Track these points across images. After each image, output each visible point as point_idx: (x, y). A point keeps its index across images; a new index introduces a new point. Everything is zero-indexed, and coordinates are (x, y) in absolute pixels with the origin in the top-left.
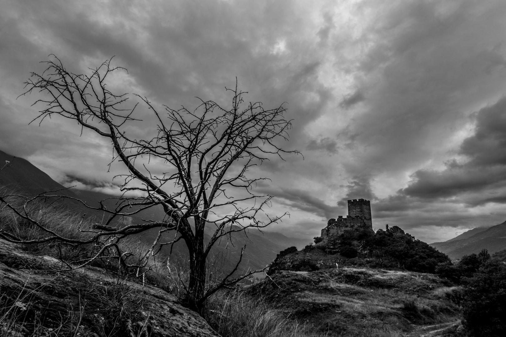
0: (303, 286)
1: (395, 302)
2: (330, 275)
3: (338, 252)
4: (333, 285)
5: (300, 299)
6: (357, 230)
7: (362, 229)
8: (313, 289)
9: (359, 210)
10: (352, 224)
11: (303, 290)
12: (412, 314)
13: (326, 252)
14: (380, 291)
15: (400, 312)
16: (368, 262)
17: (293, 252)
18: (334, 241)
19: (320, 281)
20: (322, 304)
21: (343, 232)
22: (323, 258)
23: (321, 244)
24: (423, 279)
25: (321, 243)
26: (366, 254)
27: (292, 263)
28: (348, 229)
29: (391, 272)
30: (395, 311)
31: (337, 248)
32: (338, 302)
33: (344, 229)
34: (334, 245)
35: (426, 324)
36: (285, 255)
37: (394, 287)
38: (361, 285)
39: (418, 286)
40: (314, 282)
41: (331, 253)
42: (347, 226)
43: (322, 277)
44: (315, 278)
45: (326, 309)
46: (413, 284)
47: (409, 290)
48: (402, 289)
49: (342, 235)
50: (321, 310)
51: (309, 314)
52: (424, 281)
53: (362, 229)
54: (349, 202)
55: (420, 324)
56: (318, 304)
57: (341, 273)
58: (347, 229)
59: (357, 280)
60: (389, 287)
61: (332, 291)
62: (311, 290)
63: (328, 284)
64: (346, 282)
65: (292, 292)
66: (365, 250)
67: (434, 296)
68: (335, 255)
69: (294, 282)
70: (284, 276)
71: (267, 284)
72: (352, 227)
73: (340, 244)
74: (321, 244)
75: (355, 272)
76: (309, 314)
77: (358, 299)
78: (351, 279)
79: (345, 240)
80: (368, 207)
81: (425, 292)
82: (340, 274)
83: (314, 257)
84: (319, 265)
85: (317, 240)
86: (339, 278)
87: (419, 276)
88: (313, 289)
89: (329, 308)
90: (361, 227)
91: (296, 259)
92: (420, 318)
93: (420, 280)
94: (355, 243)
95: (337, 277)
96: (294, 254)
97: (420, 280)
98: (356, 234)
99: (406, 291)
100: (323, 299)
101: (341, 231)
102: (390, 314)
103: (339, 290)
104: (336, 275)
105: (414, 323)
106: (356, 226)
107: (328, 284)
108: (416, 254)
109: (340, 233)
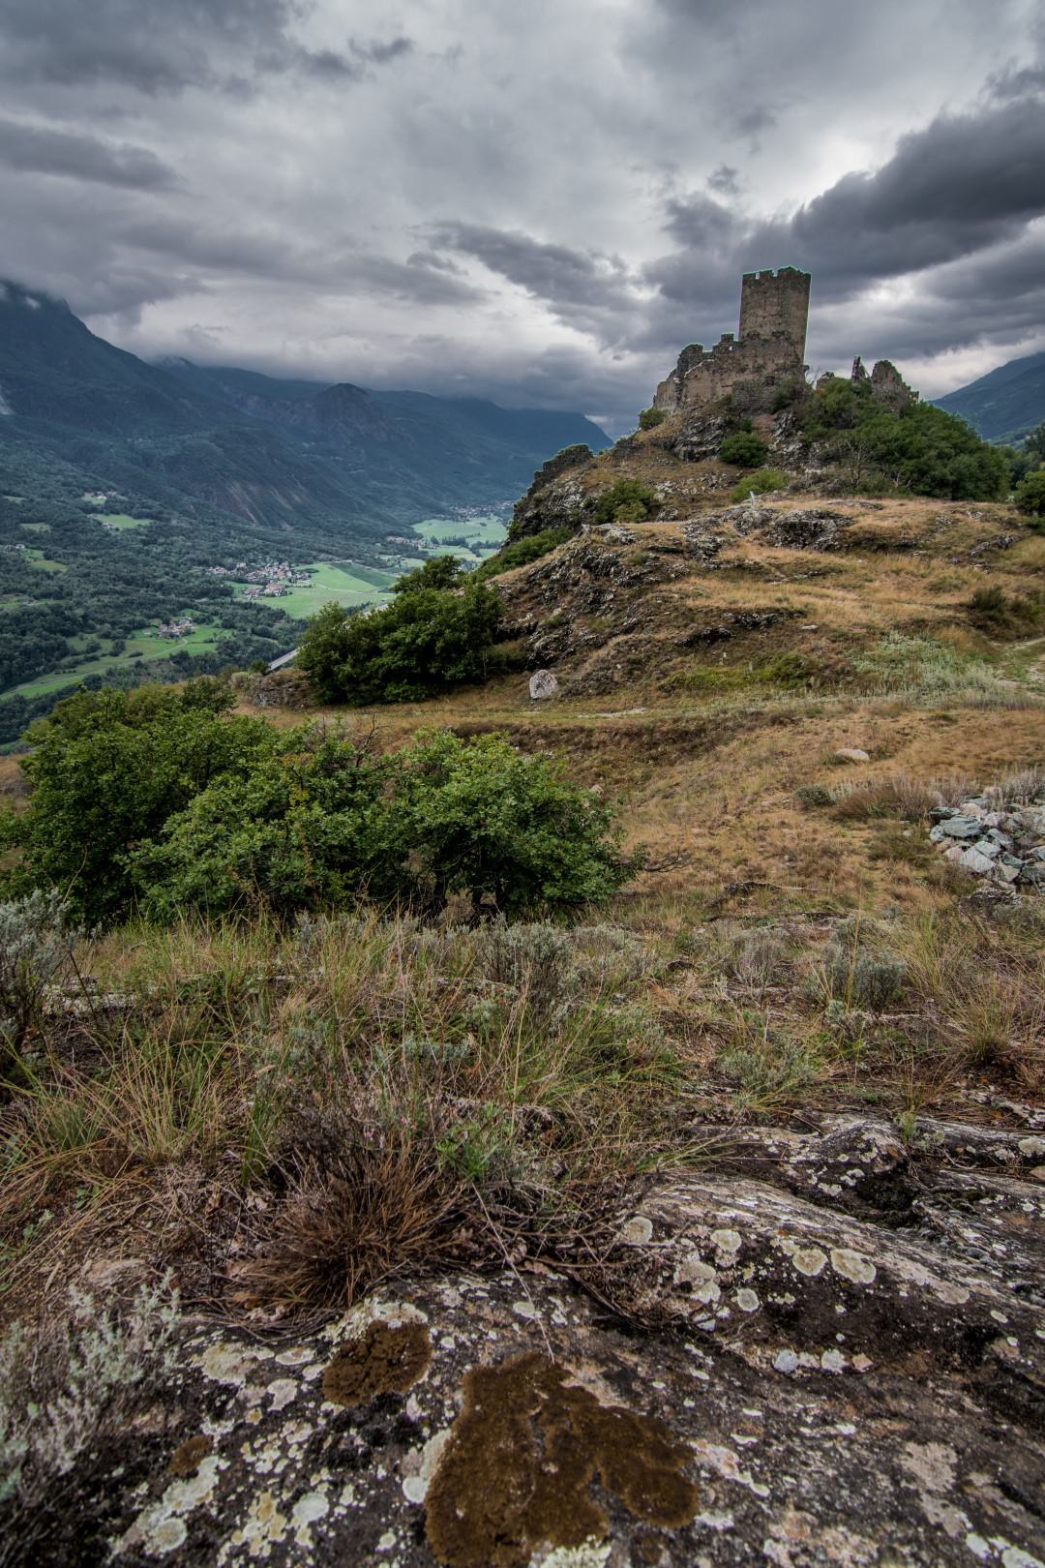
0: (678, 563)
1: (937, 588)
2: (739, 526)
3: (713, 452)
4: (755, 554)
5: (690, 603)
6: (771, 381)
7: (787, 377)
8: (708, 570)
9: (775, 310)
10: (760, 361)
11: (681, 576)
12: (991, 618)
13: (676, 455)
14: (889, 561)
15: (962, 615)
16: (818, 480)
17: (581, 462)
18: (703, 420)
19: (718, 546)
20: (759, 611)
21: (729, 390)
22: (666, 473)
23: (658, 431)
24: (984, 519)
25: (662, 427)
26: (792, 454)
27: (583, 495)
28: (747, 377)
29: (892, 505)
30: (951, 613)
31: (710, 443)
32: (797, 602)
33: (735, 377)
34: (701, 432)
35: (1019, 638)
36: (559, 472)
37: (916, 547)
38: (829, 549)
39: (980, 541)
40: (706, 551)
41: (691, 457)
42: (743, 370)
43: (720, 534)
44: (704, 539)
45: (769, 623)
46: (963, 537)
47: (957, 554)
48: (935, 551)
49: (728, 399)
50: (756, 625)
51: (726, 637)
52: (987, 525)
53: (787, 377)
54: (748, 280)
55: (1009, 640)
56: (749, 613)
57: (769, 520)
58: (742, 378)
59: (815, 535)
60: (904, 548)
61: (757, 572)
62: (704, 573)
63: (740, 552)
64: (787, 544)
65: (651, 583)
66: (788, 444)
67: (1023, 565)
68: (704, 464)
69: (652, 555)
70: (615, 541)
71: (568, 568)
72: (758, 369)
73: (720, 427)
74: (658, 431)
75: (809, 514)
76: (726, 637)
77: (836, 586)
78: (798, 533)
79: (735, 415)
80: (802, 297)
81: (998, 557)
82: (765, 521)
83: (646, 473)
84: (660, 496)
85: (649, 421)
86: (765, 534)
87: (974, 512)
88: (708, 570)
89: (779, 620)
90: (784, 369)
91: (593, 482)
92: (1007, 624)
93: (978, 525)
94: (762, 421)
95: (757, 532)
96: (584, 467)
97: (978, 525)
98: (768, 394)
99: (950, 556)
100: (751, 597)
101: (723, 387)
102: (946, 623)
103: (778, 567)
104: (755, 526)
105: (996, 638)
106: (771, 367)
107: (740, 552)
108: (930, 447)
109: (721, 393)
